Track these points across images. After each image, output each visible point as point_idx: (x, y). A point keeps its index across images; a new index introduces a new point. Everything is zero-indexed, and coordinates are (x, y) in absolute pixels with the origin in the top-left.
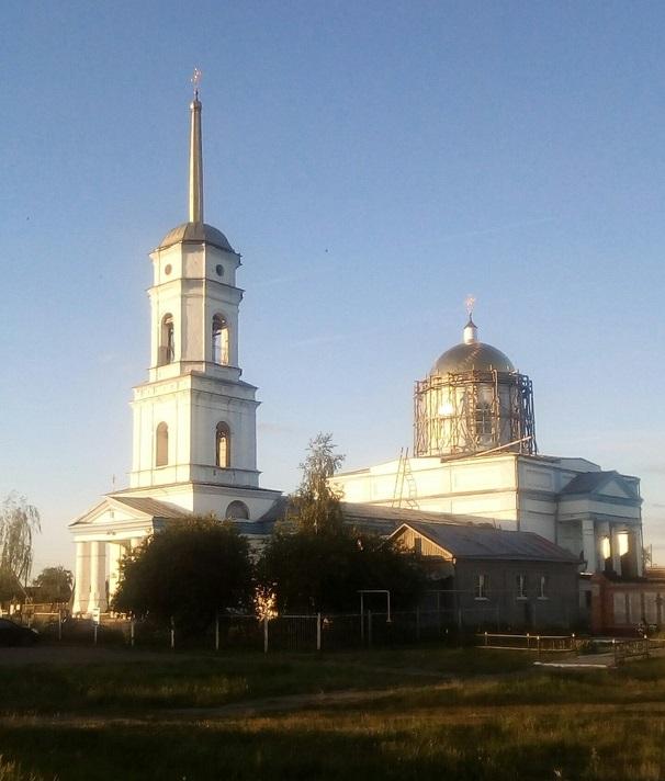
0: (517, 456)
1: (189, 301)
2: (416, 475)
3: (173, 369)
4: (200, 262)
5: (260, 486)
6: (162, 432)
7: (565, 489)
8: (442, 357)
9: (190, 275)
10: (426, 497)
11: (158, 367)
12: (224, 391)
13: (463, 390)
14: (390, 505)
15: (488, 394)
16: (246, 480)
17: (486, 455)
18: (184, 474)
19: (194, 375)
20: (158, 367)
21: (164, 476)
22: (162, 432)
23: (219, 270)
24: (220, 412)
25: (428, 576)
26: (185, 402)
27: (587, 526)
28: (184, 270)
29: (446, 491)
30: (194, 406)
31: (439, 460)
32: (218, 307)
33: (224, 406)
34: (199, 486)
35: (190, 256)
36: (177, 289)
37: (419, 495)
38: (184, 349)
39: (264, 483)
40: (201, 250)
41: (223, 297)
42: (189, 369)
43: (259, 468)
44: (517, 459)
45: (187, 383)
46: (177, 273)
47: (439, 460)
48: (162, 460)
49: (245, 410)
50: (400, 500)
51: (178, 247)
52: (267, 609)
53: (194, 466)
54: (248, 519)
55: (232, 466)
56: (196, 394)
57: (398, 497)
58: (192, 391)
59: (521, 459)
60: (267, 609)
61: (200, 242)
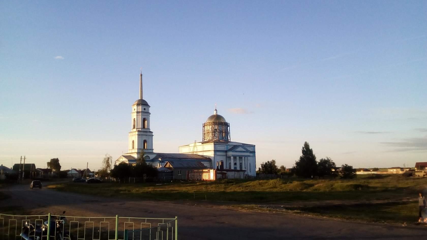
0: (214, 143)
1: (138, 116)
2: (197, 147)
3: (135, 130)
4: (140, 108)
5: (154, 152)
6: (133, 142)
7: (229, 149)
8: (210, 117)
9: (138, 111)
10: (199, 152)
11: (133, 129)
12: (145, 133)
13: (211, 126)
14: (191, 153)
15: (216, 127)
16: (150, 151)
17: (211, 142)
18: (136, 151)
19: (139, 131)
20: (133, 129)
21: (134, 151)
22: (133, 142)
23: (145, 109)
24: (145, 138)
25: (297, 176)
26: (137, 136)
27: (232, 158)
28: (137, 110)
29: (202, 150)
30: (138, 138)
31: (201, 143)
32: (144, 117)
33: (145, 137)
34: (138, 153)
35: (139, 107)
36: (136, 114)
37: (198, 151)
38: (137, 127)
39: (154, 151)
40: (140, 106)
41: (146, 115)
42: (138, 130)
43: (153, 148)
44: (214, 144)
45: (137, 133)
46: (136, 111)
47: (201, 143)
48: (133, 148)
49: (150, 137)
50: (194, 152)
51: (136, 105)
52: (172, 181)
53: (138, 149)
54: (150, 159)
55: (147, 148)
56: (139, 135)
57: (193, 151)
58: (138, 135)
59: (215, 143)
60: (172, 181)
61: (140, 104)
